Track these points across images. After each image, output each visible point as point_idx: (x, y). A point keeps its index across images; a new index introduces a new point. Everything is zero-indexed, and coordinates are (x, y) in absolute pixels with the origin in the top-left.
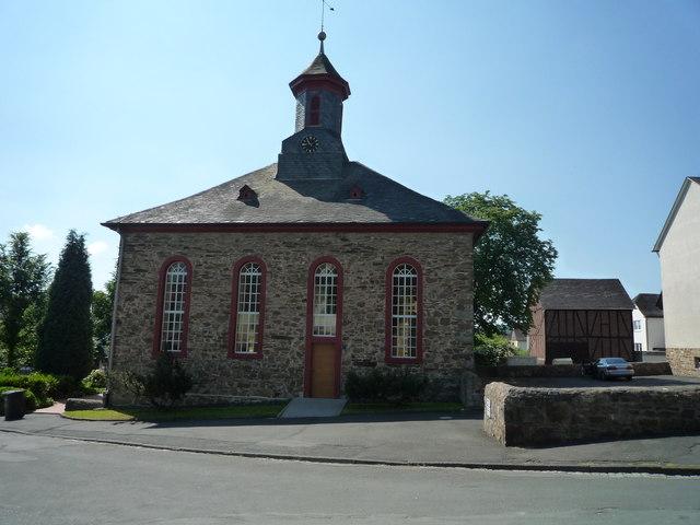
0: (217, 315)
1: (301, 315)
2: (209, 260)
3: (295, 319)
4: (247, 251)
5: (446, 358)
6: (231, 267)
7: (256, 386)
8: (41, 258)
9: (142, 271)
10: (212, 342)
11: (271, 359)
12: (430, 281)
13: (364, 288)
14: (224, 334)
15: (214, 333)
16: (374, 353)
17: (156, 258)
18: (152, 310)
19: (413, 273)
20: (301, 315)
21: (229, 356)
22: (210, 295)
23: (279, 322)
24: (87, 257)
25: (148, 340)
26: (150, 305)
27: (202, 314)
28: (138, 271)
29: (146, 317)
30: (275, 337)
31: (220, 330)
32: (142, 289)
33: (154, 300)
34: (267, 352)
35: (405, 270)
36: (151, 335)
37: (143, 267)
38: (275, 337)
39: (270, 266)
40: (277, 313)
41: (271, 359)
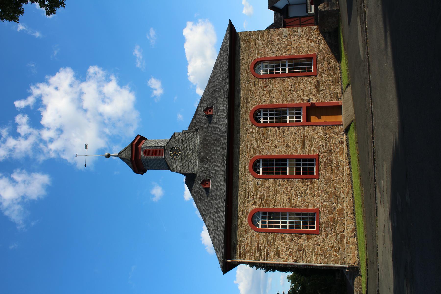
0: (289, 188)
1: (288, 130)
2: (251, 196)
3: (292, 133)
4: (245, 169)
5: (312, 41)
6: (256, 181)
7: (337, 157)
8: (7, 132)
9: (258, 245)
10: (308, 191)
11: (318, 148)
12: (265, 53)
13: (270, 92)
14: (303, 182)
15: (302, 189)
16: (310, 82)
17: (249, 235)
18: (287, 237)
19: (260, 112)
20: (288, 130)
21: (318, 179)
22: (276, 193)
23: (294, 145)
24: (185, 42)
25: (308, 239)
26: (283, 238)
27: (289, 198)
28: (258, 248)
29: (292, 240)
30: (304, 146)
31: (300, 185)
32: (271, 244)
33: (280, 236)
34: (314, 151)
35: (258, 117)
36: (304, 237)
37: (255, 244)
38: (304, 146)
39: (255, 154)
40: (287, 146)
41: (318, 148)
